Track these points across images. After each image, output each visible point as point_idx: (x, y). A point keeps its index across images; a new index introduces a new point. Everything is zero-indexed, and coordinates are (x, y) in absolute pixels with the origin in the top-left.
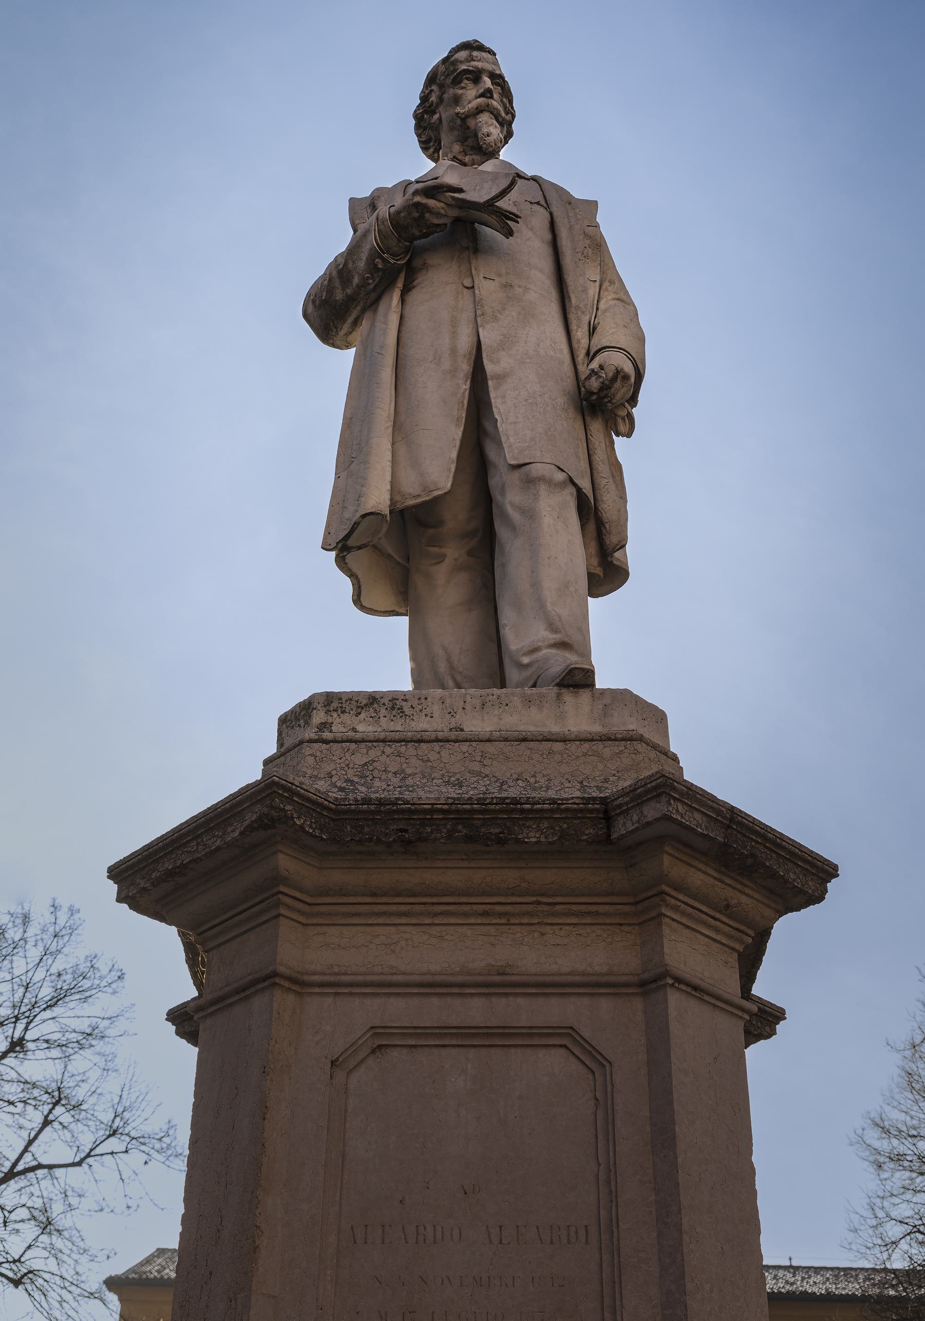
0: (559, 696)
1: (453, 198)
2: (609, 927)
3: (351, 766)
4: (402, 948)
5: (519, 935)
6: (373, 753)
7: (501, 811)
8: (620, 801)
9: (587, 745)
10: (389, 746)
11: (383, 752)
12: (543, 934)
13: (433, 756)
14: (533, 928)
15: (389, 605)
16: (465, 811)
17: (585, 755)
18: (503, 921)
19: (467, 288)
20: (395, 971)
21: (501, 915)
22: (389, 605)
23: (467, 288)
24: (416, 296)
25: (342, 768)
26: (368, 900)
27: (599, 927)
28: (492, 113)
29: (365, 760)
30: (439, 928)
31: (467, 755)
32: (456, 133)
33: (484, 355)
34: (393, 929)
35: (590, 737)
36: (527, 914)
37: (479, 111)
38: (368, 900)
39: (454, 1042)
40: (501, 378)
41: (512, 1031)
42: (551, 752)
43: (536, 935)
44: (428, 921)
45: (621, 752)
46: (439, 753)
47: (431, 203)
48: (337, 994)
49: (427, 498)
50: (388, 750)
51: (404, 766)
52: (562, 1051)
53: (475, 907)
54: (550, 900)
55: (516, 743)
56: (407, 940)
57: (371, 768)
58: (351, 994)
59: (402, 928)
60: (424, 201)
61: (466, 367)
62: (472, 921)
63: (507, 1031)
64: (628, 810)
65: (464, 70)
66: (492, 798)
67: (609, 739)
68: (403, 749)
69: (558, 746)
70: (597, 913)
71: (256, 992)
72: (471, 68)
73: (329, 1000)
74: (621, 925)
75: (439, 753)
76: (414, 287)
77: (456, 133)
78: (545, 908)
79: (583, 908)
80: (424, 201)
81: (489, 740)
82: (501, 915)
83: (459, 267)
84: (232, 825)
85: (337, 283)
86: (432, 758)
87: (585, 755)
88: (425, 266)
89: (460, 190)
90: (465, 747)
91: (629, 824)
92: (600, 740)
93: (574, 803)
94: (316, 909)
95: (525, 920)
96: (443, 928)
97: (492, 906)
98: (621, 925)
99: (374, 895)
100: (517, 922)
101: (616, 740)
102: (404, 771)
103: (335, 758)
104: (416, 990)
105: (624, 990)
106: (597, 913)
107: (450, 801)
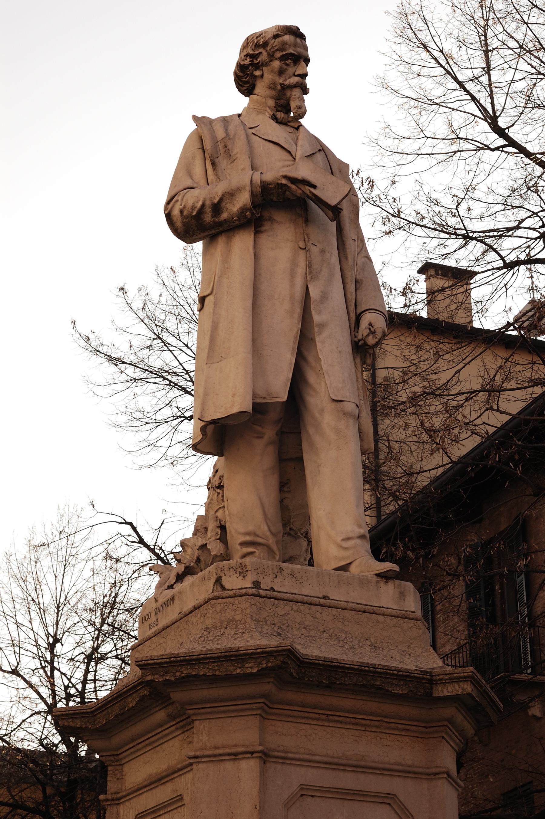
0: (378, 582)
1: (310, 192)
2: (412, 738)
3: (276, 615)
4: (314, 739)
5: (370, 738)
6: (288, 608)
7: (382, 673)
8: (441, 677)
9: (395, 620)
10: (295, 605)
11: (292, 608)
12: (381, 739)
13: (318, 615)
14: (376, 734)
15: (212, 451)
16: (366, 671)
17: (395, 626)
18: (363, 729)
19: (301, 248)
20: (311, 752)
21: (363, 725)
22: (212, 451)
23: (301, 248)
24: (264, 239)
25: (272, 616)
26: (299, 709)
27: (407, 737)
28: (302, 89)
29: (283, 612)
30: (331, 729)
31: (335, 617)
32: (273, 93)
33: (312, 306)
34: (308, 726)
35: (397, 615)
36: (377, 727)
37: (295, 86)
38: (299, 709)
39: (337, 796)
40: (322, 326)
41: (367, 793)
42: (378, 622)
43: (378, 738)
44: (327, 724)
45: (412, 627)
46: (321, 613)
47: (293, 187)
48: (283, 763)
49: (270, 401)
50: (295, 608)
51: (304, 619)
52: (387, 806)
53: (352, 720)
54: (388, 720)
55: (360, 613)
56: (316, 734)
57: (287, 618)
58: (290, 764)
59: (313, 726)
60: (290, 185)
61: (298, 310)
62: (348, 726)
63: (364, 793)
64: (446, 682)
65: (291, 53)
66: (379, 665)
67: (406, 618)
68: (302, 608)
69: (381, 618)
70: (409, 730)
71: (244, 758)
72: (295, 53)
73: (279, 766)
74: (418, 737)
75: (321, 613)
76: (262, 232)
77: (273, 93)
78: (385, 724)
79: (403, 726)
80: (290, 185)
81: (346, 609)
82: (363, 725)
83: (295, 229)
84: (250, 663)
85: (208, 210)
86: (318, 617)
87: (395, 626)
88: (271, 220)
89: (315, 187)
90: (334, 611)
91: (445, 691)
92: (401, 618)
93: (417, 674)
94: (274, 711)
95: (374, 730)
96: (333, 729)
97: (360, 720)
98: (418, 737)
99: (303, 706)
100: (369, 730)
101: (409, 618)
102: (304, 623)
103: (267, 609)
104: (322, 766)
105: (420, 776)
106: (409, 730)
107: (359, 664)
